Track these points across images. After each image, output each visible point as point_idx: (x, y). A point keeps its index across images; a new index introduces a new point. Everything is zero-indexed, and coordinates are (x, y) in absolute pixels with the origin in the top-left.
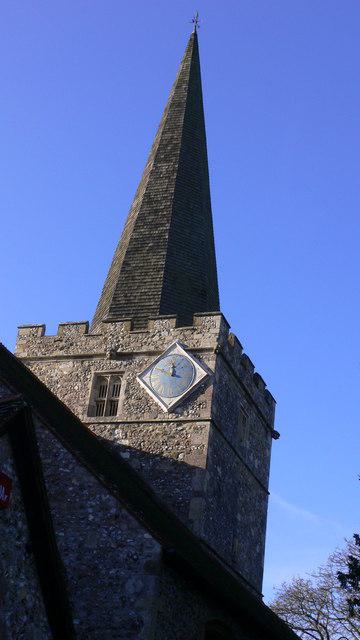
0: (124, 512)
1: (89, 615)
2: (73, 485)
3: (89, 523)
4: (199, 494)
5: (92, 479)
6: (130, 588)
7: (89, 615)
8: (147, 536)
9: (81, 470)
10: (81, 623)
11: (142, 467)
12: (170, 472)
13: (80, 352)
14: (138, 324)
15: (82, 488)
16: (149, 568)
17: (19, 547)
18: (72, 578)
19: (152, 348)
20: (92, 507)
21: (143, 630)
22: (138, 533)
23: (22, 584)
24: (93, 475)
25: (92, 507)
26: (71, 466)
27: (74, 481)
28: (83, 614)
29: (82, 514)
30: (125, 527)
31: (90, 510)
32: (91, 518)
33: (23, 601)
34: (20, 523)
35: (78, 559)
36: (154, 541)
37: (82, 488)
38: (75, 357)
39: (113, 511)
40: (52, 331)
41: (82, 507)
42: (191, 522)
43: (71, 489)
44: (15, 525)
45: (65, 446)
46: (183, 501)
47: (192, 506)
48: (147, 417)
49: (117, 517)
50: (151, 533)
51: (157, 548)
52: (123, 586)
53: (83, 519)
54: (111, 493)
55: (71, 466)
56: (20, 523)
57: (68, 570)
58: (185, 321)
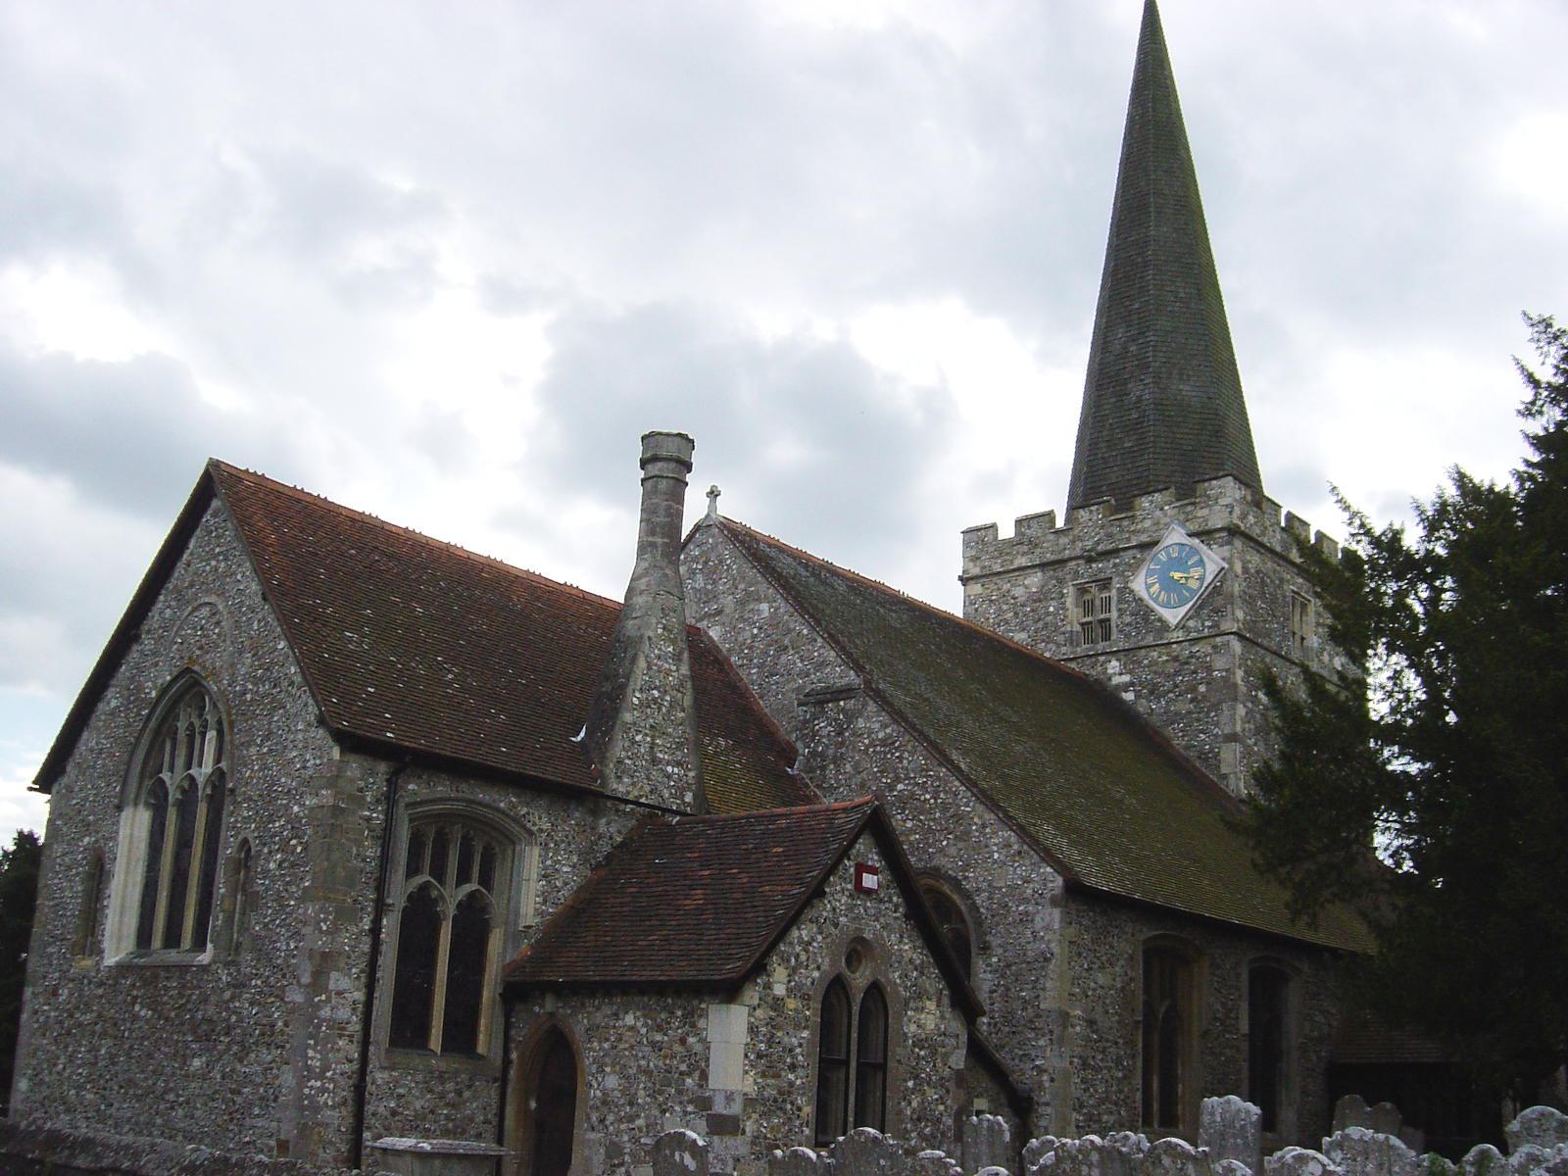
0: (1025, 847)
1: (1005, 952)
2: (976, 824)
3: (995, 862)
4: (1232, 738)
5: (992, 816)
6: (1039, 923)
7: (1005, 952)
8: (1049, 869)
9: (980, 808)
10: (999, 961)
11: (1152, 710)
12: (1189, 712)
13: (1049, 557)
14: (1124, 505)
15: (984, 826)
16: (1054, 902)
17: (896, 918)
18: (986, 918)
19: (1144, 538)
20: (995, 845)
21: (1054, 961)
22: (1040, 867)
23: (907, 947)
24: (993, 812)
25: (995, 845)
26: (971, 804)
27: (976, 820)
28: (1000, 951)
29: (987, 853)
30: (1028, 862)
31: (995, 848)
32: (996, 856)
33: (911, 961)
34: (895, 899)
35: (989, 899)
36: (1056, 875)
37: (984, 826)
38: (1043, 566)
39: (1016, 847)
40: (1007, 531)
41: (986, 846)
42: (1225, 777)
43: (974, 828)
44: (890, 901)
45: (963, 784)
46: (1211, 750)
47: (1223, 755)
48: (1150, 640)
49: (1020, 853)
50: (1052, 867)
51: (1060, 881)
52: (1032, 921)
53: (989, 858)
54: (1012, 830)
55: (971, 804)
56: (895, 899)
57: (982, 910)
58: (1187, 492)
